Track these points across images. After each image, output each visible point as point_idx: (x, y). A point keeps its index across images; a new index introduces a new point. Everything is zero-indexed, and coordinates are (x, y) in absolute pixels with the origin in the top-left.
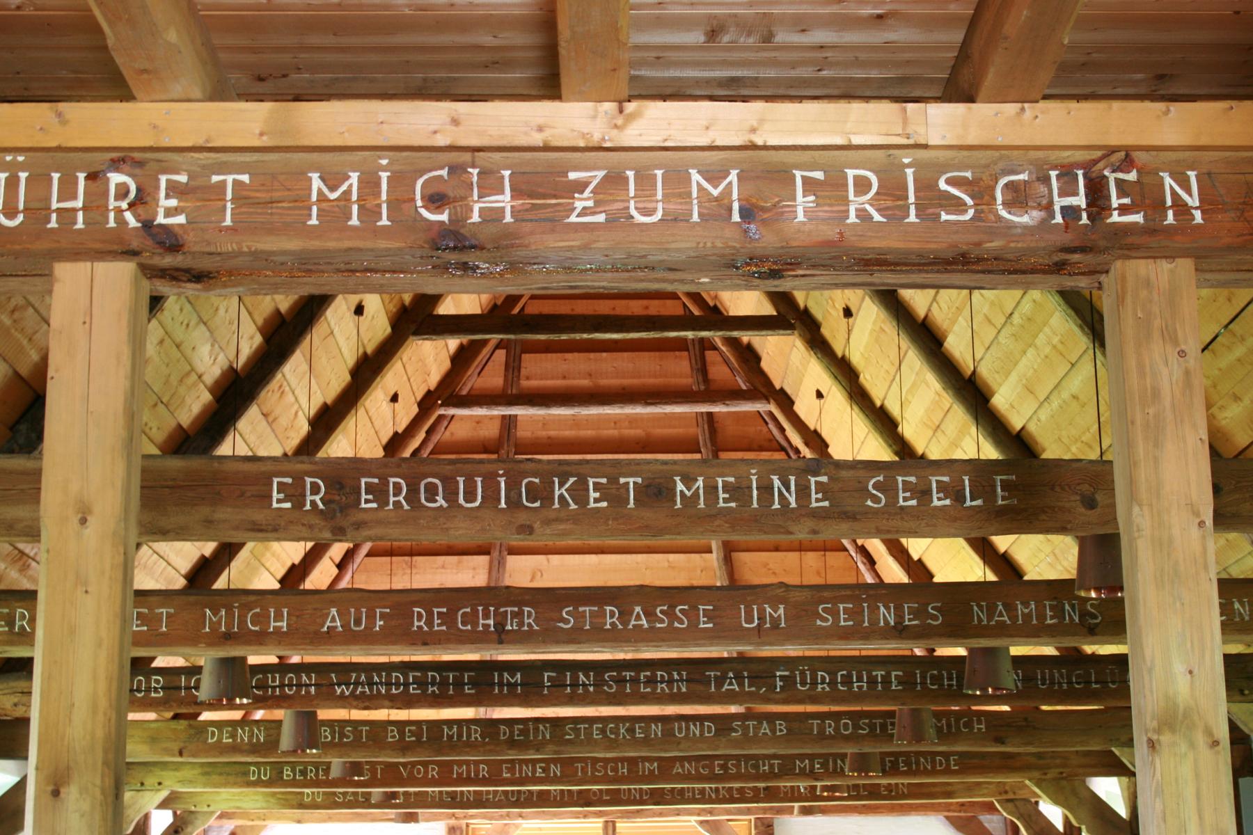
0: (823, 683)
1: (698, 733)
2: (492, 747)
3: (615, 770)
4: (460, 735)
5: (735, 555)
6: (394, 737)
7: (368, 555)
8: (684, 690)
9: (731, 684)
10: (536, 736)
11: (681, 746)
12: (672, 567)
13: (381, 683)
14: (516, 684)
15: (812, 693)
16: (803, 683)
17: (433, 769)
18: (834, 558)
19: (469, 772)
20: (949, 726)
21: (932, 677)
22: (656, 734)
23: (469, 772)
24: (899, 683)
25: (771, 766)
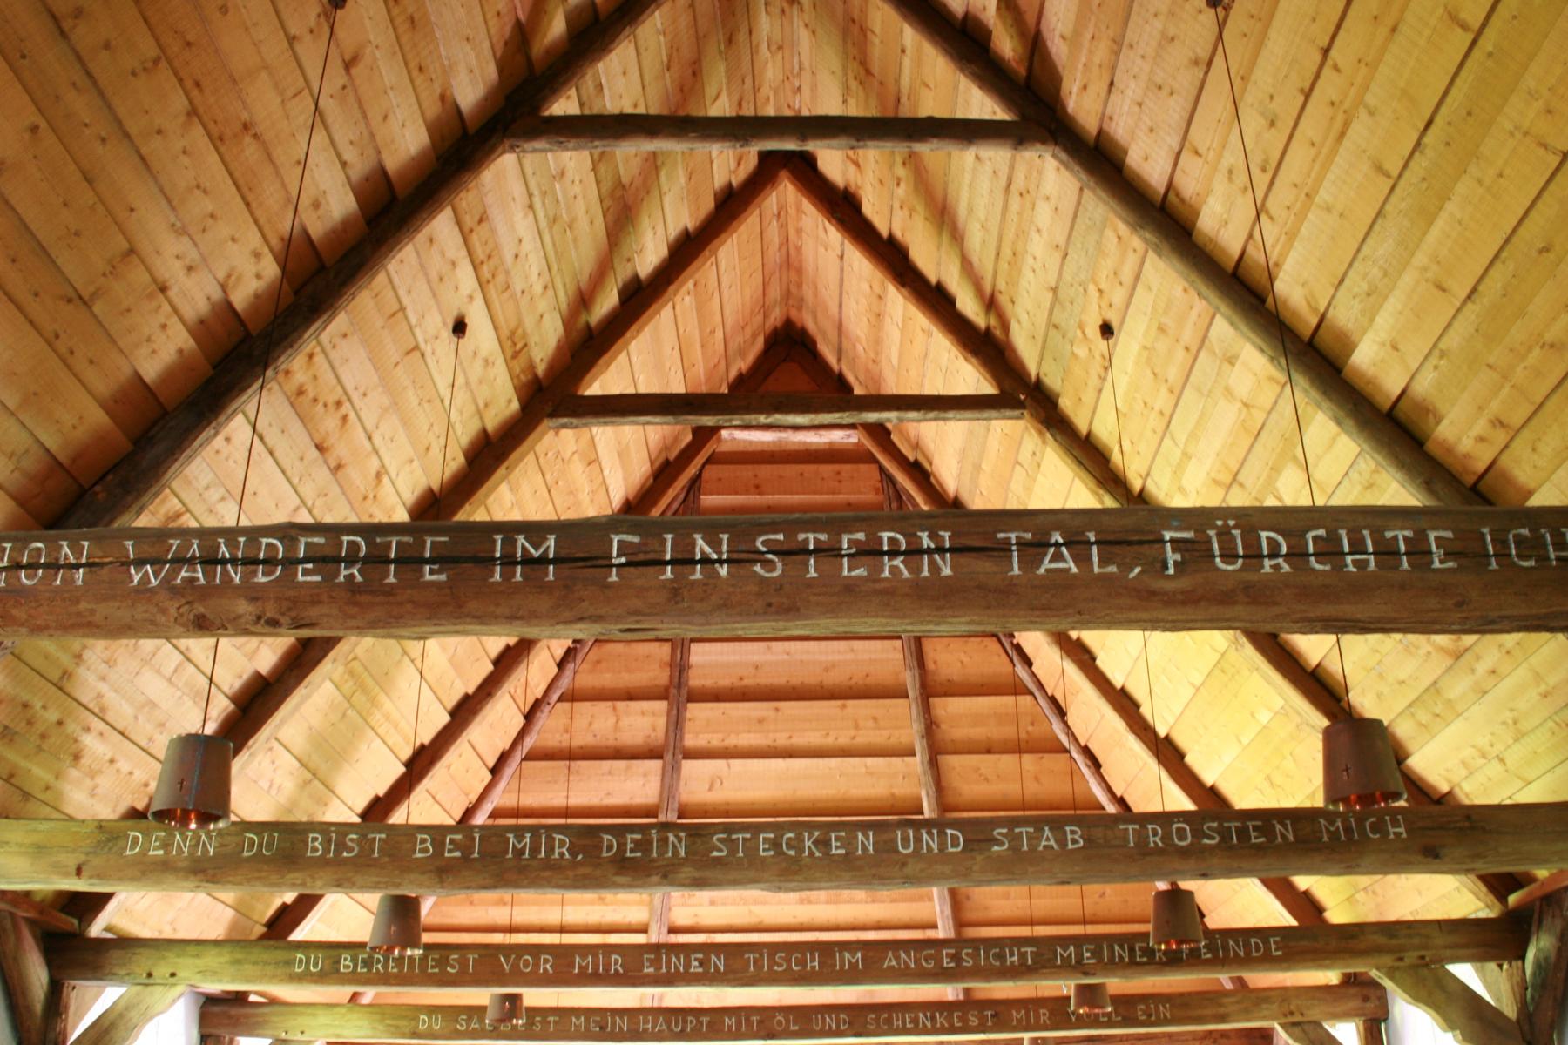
0: (1274, 554)
1: (935, 847)
2: (587, 870)
3: (802, 962)
4: (535, 850)
6: (426, 850)
8: (947, 571)
9: (1058, 557)
10: (662, 853)
11: (909, 870)
13: (234, 561)
14: (543, 560)
15: (1251, 577)
16: (1230, 556)
17: (546, 961)
19: (596, 965)
20: (1348, 830)
21: (1519, 541)
22: (865, 848)
23: (596, 965)
24: (1449, 555)
25: (1022, 956)
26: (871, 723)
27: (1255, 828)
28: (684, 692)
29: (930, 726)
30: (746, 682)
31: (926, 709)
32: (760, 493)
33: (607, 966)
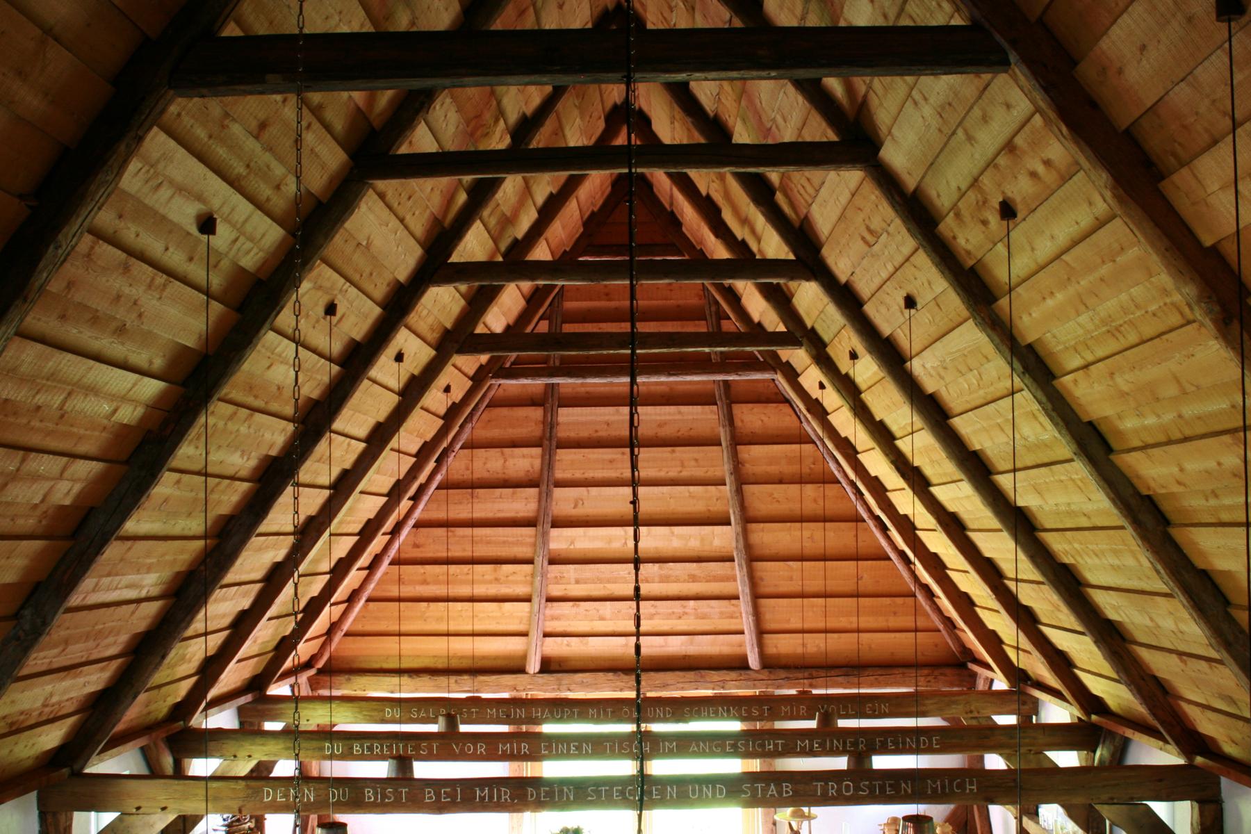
5: (745, 487)
7: (437, 488)
12: (691, 496)
18: (831, 490)
19: (512, 749)
20: (943, 787)
23: (512, 749)
25: (776, 745)
26: (693, 463)
27: (890, 786)
28: (554, 443)
29: (737, 464)
30: (600, 434)
31: (734, 456)
32: (609, 300)
33: (519, 750)
